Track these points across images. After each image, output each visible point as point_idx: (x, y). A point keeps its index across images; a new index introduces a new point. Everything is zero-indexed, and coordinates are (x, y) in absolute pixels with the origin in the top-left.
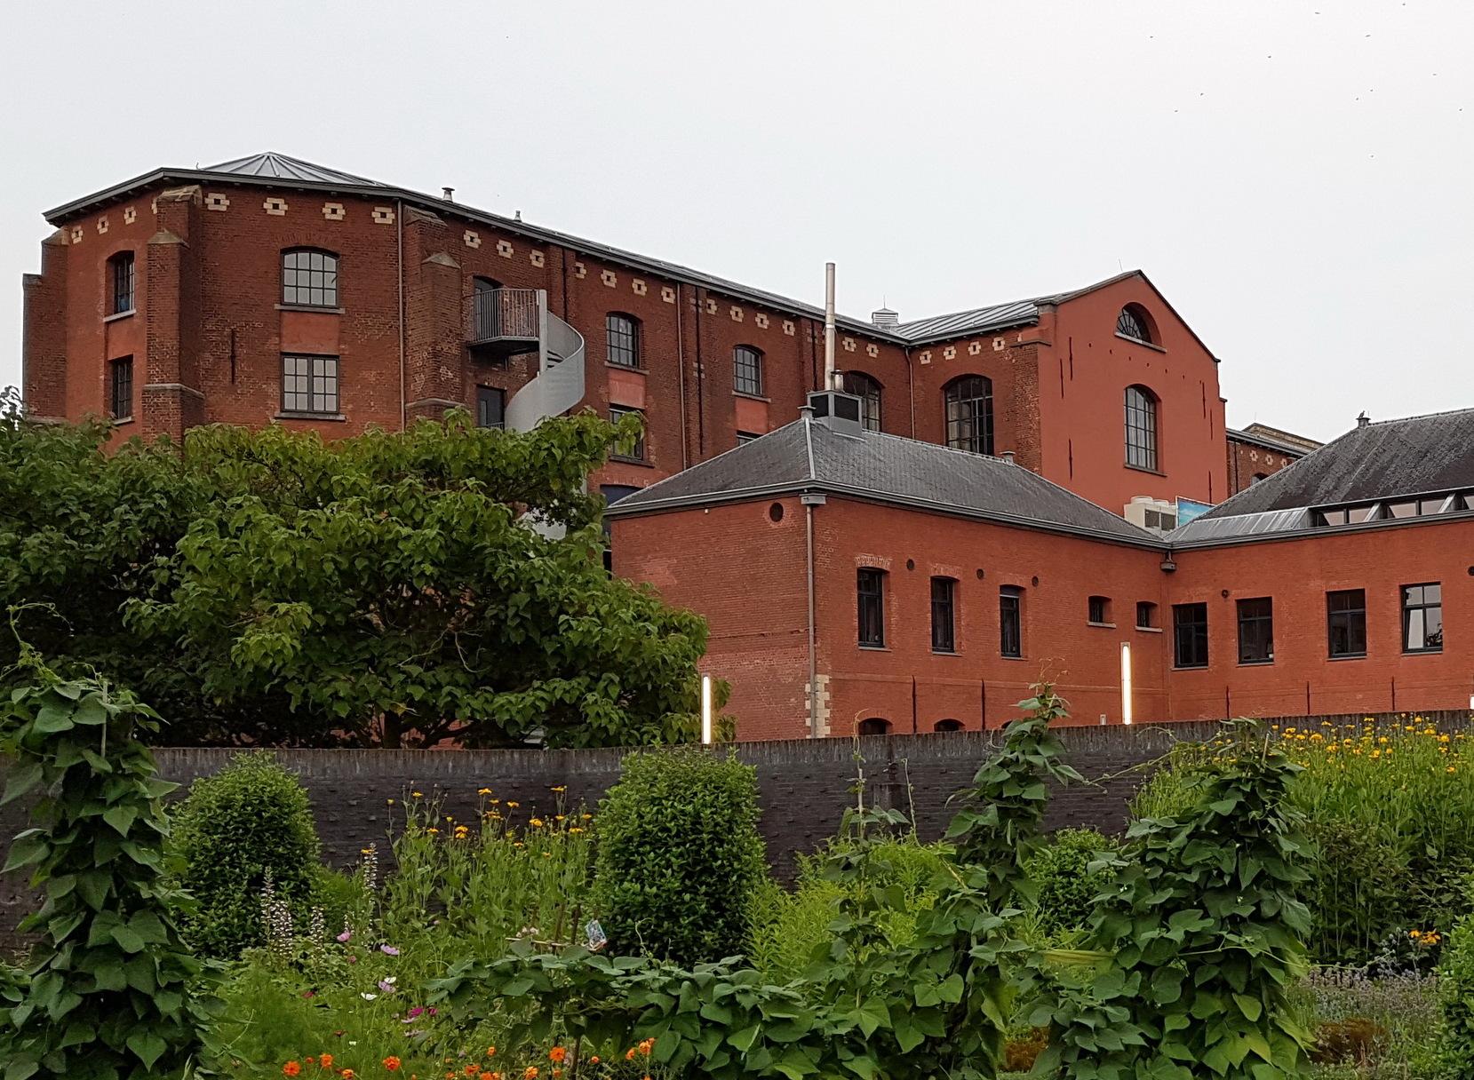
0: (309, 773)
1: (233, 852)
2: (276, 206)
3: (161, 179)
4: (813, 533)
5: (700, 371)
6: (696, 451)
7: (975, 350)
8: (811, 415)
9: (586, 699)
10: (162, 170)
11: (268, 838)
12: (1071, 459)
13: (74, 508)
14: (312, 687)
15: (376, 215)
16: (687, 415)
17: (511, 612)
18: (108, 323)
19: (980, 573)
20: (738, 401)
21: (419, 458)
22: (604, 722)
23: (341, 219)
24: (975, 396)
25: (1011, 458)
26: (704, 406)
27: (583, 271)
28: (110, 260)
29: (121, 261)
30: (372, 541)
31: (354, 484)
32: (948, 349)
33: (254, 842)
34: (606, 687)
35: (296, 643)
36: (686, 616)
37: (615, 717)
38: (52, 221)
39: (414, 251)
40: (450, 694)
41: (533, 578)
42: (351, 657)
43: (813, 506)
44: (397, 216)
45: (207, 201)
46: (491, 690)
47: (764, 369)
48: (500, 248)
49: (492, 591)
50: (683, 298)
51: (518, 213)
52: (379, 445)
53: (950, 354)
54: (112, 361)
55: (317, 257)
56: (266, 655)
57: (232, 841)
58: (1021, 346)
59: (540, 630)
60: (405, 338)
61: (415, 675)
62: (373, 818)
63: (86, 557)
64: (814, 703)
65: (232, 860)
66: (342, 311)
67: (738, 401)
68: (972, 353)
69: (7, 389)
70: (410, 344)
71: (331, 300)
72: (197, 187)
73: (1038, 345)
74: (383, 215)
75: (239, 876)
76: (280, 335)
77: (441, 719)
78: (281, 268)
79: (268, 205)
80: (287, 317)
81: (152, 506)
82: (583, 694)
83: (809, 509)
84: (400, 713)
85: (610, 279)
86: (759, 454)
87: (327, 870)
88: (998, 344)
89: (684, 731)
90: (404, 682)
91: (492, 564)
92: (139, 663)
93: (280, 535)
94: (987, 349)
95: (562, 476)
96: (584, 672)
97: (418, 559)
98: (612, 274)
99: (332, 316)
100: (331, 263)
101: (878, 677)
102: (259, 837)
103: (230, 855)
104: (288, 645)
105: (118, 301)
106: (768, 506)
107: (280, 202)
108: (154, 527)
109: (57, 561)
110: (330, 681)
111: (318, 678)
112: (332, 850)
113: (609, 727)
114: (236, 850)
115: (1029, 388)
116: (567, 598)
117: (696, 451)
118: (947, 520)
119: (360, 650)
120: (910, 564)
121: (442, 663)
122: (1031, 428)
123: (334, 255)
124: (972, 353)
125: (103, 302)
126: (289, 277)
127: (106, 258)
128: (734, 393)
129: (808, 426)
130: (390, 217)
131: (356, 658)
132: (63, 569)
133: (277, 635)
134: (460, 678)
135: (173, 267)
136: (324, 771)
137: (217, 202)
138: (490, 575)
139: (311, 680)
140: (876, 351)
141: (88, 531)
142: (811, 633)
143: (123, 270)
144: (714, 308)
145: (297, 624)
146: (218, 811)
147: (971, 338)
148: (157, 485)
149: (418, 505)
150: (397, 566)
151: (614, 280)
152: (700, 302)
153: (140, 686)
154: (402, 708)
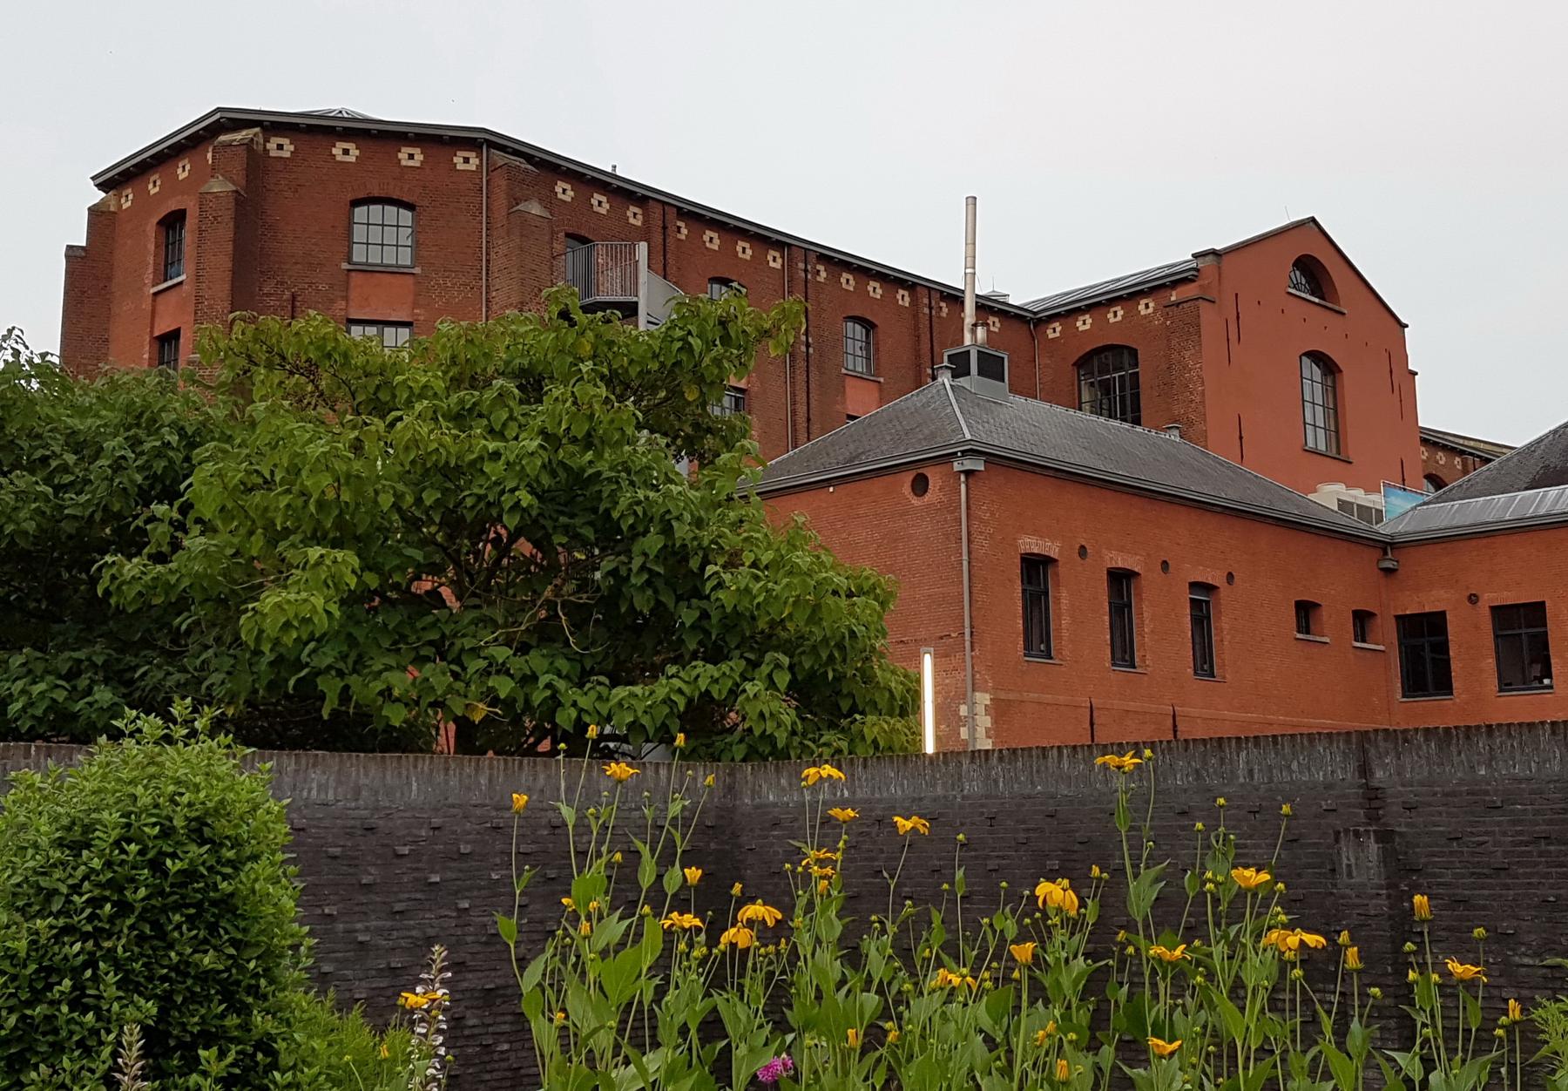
0: (331, 796)
1: (85, 965)
2: (346, 152)
3: (218, 120)
4: (968, 508)
5: (808, 345)
6: (802, 436)
7: (1115, 316)
8: (949, 375)
9: (744, 691)
10: (219, 110)
11: (178, 927)
12: (1241, 438)
13: (57, 449)
14: (354, 680)
15: (458, 160)
16: (793, 394)
17: (637, 563)
18: (155, 294)
19: (1165, 565)
20: (849, 382)
21: (511, 362)
22: (770, 726)
23: (418, 165)
24: (1116, 370)
25: (1176, 432)
26: (812, 386)
27: (684, 231)
28: (160, 223)
29: (173, 222)
30: (447, 463)
31: (425, 387)
32: (1081, 318)
33: (141, 939)
34: (770, 676)
35: (334, 609)
36: (867, 578)
37: (785, 718)
38: (100, 186)
39: (501, 201)
40: (549, 686)
41: (668, 512)
42: (413, 638)
43: (968, 473)
44: (481, 160)
45: (269, 146)
46: (607, 681)
47: (877, 344)
48: (594, 202)
49: (611, 536)
50: (790, 264)
51: (615, 167)
52: (459, 337)
53: (1084, 324)
54: (157, 338)
55: (391, 210)
56: (287, 625)
57: (85, 937)
58: (1178, 305)
59: (675, 591)
60: (488, 301)
61: (500, 661)
62: (436, 878)
63: (66, 512)
64: (973, 730)
65: (78, 987)
66: (417, 270)
67: (848, 380)
68: (1112, 320)
69: (10, 331)
70: (495, 307)
71: (406, 258)
72: (257, 130)
73: (1201, 303)
74: (466, 160)
75: (94, 1032)
76: (346, 298)
77: (528, 737)
78: (350, 223)
79: (337, 151)
80: (356, 279)
81: (158, 444)
82: (738, 685)
83: (963, 478)
84: (477, 718)
85: (713, 241)
86: (891, 421)
87: (324, 1015)
88: (1146, 307)
89: (882, 744)
90: (486, 673)
91: (613, 493)
92: (134, 661)
93: (317, 449)
94: (1131, 314)
95: (700, 380)
96: (737, 653)
97: (510, 485)
98: (715, 235)
99: (407, 277)
100: (406, 216)
101: (1048, 698)
102: (156, 925)
103: (76, 973)
104: (320, 610)
105: (169, 263)
106: (908, 478)
107: (351, 146)
108: (159, 472)
109: (23, 514)
110: (380, 672)
111: (366, 667)
112: (361, 938)
113: (776, 734)
114: (92, 963)
115: (1188, 353)
116: (712, 542)
117: (802, 436)
118: (1124, 496)
119: (424, 629)
120: (1083, 551)
121: (538, 646)
122: (1192, 401)
123: (410, 207)
124: (1112, 320)
125: (151, 269)
126: (359, 233)
127: (155, 220)
128: (844, 371)
129: (948, 387)
130: (474, 162)
131: (419, 639)
132: (30, 526)
133: (304, 595)
134: (563, 664)
135: (227, 216)
136: (357, 792)
137: (280, 147)
138: (607, 512)
139: (354, 671)
140: (998, 325)
141: (73, 478)
142: (967, 637)
143: (174, 237)
144: (823, 274)
145: (335, 581)
146: (56, 854)
147: (1112, 302)
148: (167, 417)
149: (511, 418)
150: (480, 498)
151: (717, 241)
152: (809, 267)
153: (130, 694)
154: (480, 712)
